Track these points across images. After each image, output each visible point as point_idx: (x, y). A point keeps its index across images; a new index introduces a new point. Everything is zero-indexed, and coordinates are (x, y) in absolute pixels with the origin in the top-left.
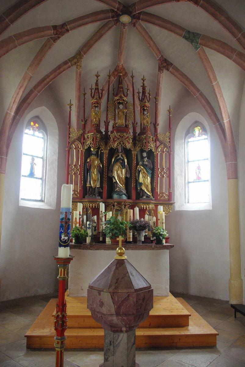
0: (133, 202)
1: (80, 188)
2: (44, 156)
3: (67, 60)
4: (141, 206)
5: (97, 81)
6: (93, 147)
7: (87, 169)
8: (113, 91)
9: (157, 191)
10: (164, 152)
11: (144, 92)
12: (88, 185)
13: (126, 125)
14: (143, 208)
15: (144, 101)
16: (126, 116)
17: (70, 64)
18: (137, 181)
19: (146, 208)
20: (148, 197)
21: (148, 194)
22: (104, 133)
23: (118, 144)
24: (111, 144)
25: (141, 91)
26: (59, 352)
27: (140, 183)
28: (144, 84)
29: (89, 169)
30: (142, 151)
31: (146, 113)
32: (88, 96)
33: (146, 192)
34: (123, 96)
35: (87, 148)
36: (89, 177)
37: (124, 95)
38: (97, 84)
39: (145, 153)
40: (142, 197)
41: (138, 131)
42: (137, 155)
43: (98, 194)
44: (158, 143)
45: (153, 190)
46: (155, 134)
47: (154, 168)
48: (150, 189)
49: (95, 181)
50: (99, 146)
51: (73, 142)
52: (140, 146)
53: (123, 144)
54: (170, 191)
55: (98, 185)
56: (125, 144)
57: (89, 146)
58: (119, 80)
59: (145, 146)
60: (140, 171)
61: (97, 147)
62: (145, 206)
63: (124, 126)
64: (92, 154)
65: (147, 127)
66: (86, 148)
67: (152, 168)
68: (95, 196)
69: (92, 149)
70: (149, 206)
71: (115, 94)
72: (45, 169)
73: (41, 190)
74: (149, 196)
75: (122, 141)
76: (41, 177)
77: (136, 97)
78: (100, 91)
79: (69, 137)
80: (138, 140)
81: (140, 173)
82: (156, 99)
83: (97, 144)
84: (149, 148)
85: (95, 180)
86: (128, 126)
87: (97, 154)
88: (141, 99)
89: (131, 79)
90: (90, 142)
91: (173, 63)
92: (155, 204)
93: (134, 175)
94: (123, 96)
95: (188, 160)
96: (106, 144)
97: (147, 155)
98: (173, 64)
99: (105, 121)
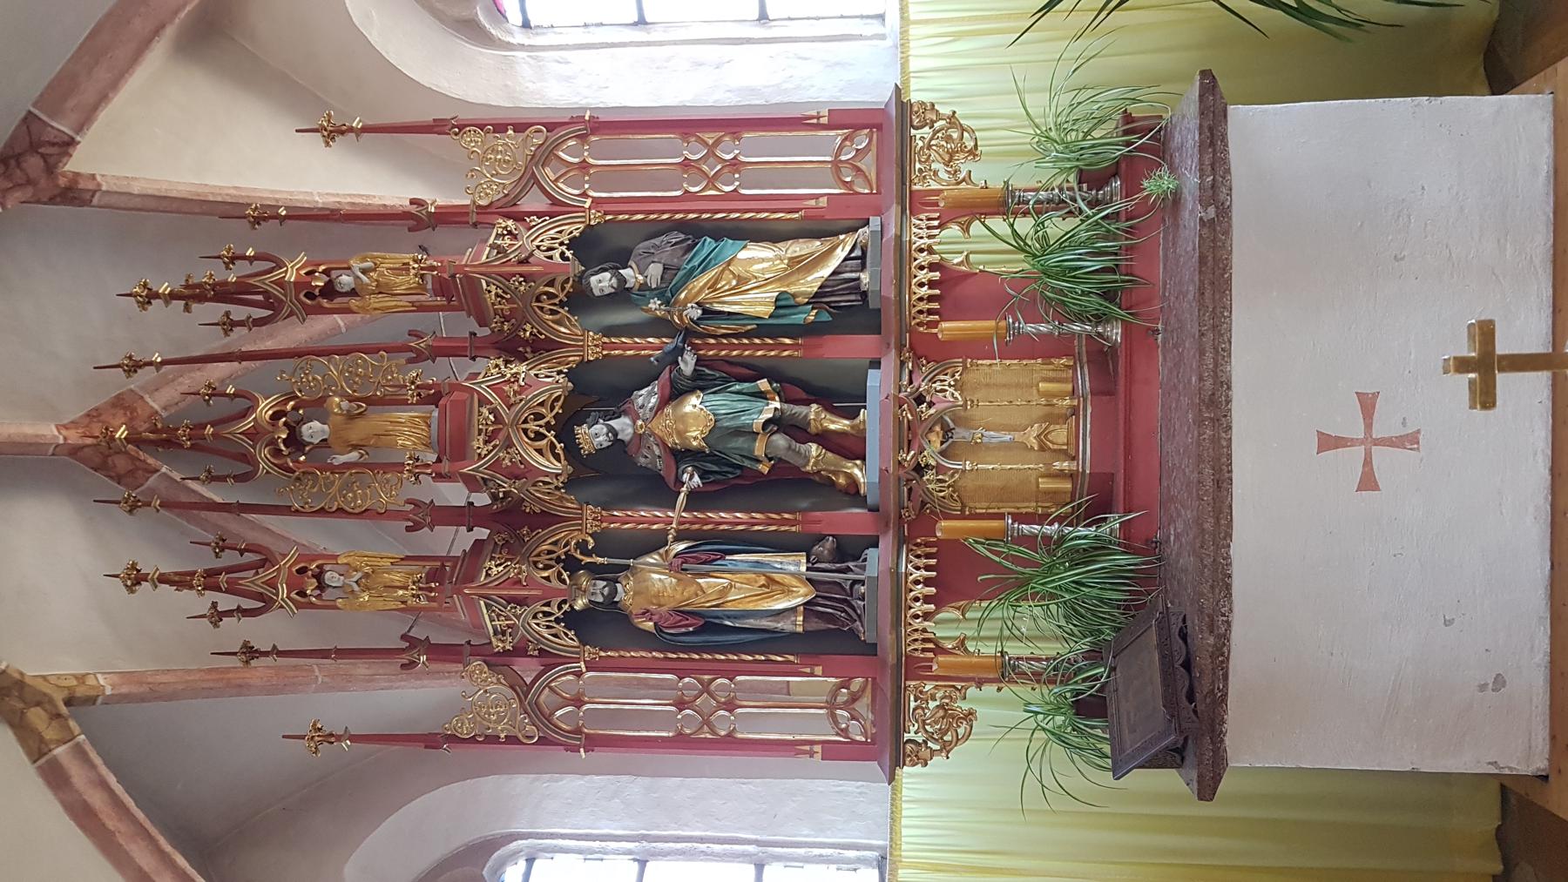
1: (818, 670)
2: (629, 852)
3: (39, 768)
4: (921, 299)
5: (163, 579)
6: (564, 602)
8: (222, 479)
9: (823, 202)
10: (584, 166)
11: (223, 293)
12: (798, 624)
13: (423, 401)
14: (932, 284)
15: (276, 291)
16: (371, 401)
17: (60, 751)
18: (764, 329)
19: (932, 267)
20: (863, 257)
21: (846, 259)
22: (482, 533)
23: (539, 451)
24: (545, 489)
25: (216, 310)
26: (464, 219)
27: (777, 308)
28: (173, 296)
30: (580, 300)
31: (346, 280)
32: (266, 630)
33: (834, 273)
34: (247, 424)
35: (571, 634)
36: (751, 623)
37: (244, 415)
38: (180, 581)
39: (593, 279)
40: (864, 294)
41: (455, 325)
42: (609, 331)
43: (851, 564)
44: (533, 202)
45: (819, 228)
46: (474, 218)
47: (682, 226)
48: (816, 245)
49: (772, 585)
50: (558, 560)
51: (540, 715)
52: (553, 312)
53: (539, 417)
54: (824, 120)
55: (798, 564)
56: (542, 404)
57: (557, 621)
58: (151, 442)
59: (549, 278)
60: (705, 311)
61: (565, 575)
62: (923, 276)
63: (436, 414)
64: (611, 602)
65: (432, 268)
66: (570, 641)
67: (682, 236)
68: (862, 582)
69: (580, 604)
70: (921, 250)
71: (242, 468)
72: (703, 847)
73: (823, 867)
74: (857, 253)
75: (525, 421)
76: (751, 869)
77: (271, 336)
78: (230, 558)
79: (512, 740)
80: (519, 327)
81: (718, 307)
82: (257, 220)
83: (545, 574)
84: (562, 254)
86: (429, 387)
87: (610, 574)
88: (267, 313)
89: (146, 374)
90: (535, 617)
91: (23, 114)
92: (903, 211)
93: (733, 347)
94: (247, 424)
95: (635, 24)
96: (546, 519)
97: (611, 264)
98: (30, 112)
99: (408, 529)
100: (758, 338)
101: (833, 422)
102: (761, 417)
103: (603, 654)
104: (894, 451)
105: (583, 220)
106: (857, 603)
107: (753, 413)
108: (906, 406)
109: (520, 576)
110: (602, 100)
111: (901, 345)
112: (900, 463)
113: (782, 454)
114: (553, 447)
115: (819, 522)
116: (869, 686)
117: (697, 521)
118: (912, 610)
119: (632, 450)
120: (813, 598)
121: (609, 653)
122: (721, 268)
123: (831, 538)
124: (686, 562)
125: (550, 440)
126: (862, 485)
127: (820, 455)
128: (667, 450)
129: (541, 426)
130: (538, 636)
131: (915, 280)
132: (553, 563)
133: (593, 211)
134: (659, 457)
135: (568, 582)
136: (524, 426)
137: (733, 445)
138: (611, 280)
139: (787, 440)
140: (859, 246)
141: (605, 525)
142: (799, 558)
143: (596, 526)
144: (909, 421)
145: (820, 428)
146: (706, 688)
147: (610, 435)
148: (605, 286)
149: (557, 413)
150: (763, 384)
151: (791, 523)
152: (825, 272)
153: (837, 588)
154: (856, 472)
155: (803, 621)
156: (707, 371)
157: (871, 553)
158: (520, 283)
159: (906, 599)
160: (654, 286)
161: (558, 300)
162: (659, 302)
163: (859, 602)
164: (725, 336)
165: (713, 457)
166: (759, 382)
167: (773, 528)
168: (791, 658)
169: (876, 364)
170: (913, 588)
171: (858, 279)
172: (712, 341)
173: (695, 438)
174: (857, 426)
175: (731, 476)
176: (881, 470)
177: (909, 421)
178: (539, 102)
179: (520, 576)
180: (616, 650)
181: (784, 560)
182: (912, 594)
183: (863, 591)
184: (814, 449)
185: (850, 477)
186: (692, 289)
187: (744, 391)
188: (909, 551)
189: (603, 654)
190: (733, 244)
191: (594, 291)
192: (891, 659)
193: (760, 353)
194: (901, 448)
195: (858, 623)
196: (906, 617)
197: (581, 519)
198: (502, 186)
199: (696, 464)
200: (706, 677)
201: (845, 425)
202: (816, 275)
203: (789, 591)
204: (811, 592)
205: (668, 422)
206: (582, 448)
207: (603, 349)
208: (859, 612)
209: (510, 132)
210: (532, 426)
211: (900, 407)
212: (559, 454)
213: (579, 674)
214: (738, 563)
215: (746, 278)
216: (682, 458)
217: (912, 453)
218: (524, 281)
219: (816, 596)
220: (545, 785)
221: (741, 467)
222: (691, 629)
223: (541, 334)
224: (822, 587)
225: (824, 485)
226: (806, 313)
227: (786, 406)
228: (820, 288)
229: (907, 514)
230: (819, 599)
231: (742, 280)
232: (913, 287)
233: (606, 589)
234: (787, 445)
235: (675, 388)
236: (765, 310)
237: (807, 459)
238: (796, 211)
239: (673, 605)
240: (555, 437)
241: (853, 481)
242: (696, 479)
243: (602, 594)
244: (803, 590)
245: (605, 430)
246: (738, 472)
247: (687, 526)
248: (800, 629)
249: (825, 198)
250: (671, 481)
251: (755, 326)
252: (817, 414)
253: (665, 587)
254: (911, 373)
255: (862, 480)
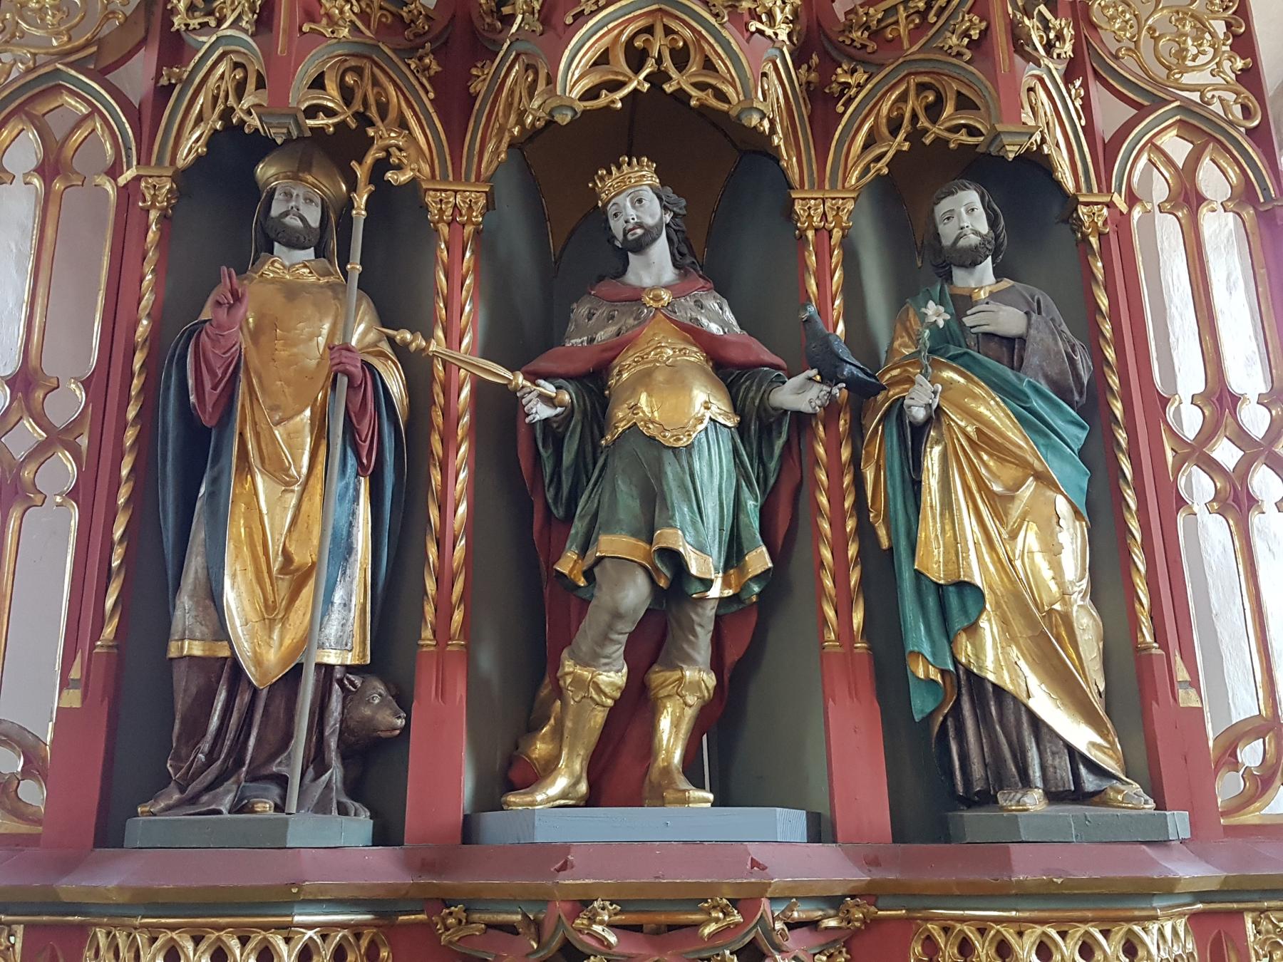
0: (859, 876)
7: (185, 410)
20: (1078, 796)
21: (1071, 750)
23: (603, 59)
29: (208, 419)
40: (987, 799)
43: (335, 773)
55: (342, 645)
56: (708, 65)
74: (1090, 782)
75: (668, 31)
81: (932, 458)
85: (298, 577)
93: (836, 496)
100: (860, 553)
101: (676, 725)
102: (689, 547)
103: (153, 215)
104: (620, 887)
105: (1084, 190)
106: (229, 792)
107: (697, 530)
108: (738, 918)
109: (324, 21)
110: (1181, 340)
111: (877, 897)
112: (587, 903)
113: (603, 597)
114: (615, 86)
115: (442, 692)
116: (23, 828)
117: (451, 419)
118: (190, 946)
119: (606, 288)
120: (250, 682)
121: (154, 227)
122: (1031, 459)
123: (400, 722)
124: (350, 385)
125: (630, 80)
126: (528, 799)
127: (599, 690)
128: (608, 355)
129: (659, 61)
130: (197, 80)
131: (1053, 932)
132: (357, 106)
133: (1105, 211)
134: (591, 341)
135: (310, 122)
136: (659, 31)
137: (622, 486)
138: (976, 233)
139: (635, 611)
140: (1105, 784)
141: (444, 229)
142: (357, 649)
143: (441, 211)
144: (697, 926)
145: (663, 693)
146: (56, 438)
147: (639, 231)
148: (960, 219)
149: (690, 97)
150: (759, 560)
151: (441, 630)
152: (1045, 704)
153: (273, 738)
154: (560, 784)
155: (191, 657)
156: (779, 444)
157: (360, 826)
158: (966, 34)
159: (220, 928)
160: (968, 321)
161: (927, 124)
162: (941, 324)
163: (228, 799)
164: (859, 481)
165: (590, 455)
166: (764, 549)
167: (431, 586)
168: (109, 631)
169: (819, 830)
170: (250, 946)
171: (1026, 783)
172: (845, 454)
173: (635, 408)
174: (672, 782)
175: (550, 496)
176: (566, 848)
177: (697, 926)
178: (1166, 244)
179: (324, 21)
180: (161, 244)
181: (354, 612)
182: (234, 944)
183: (259, 807)
184: (613, 678)
185: (548, 769)
186: (975, 397)
187: (742, 517)
188: (357, 930)
189: (153, 215)
190: (1081, 489)
191: (949, 199)
192: (70, 886)
193: (826, 554)
194: (624, 905)
195: (176, 796)
196: (173, 928)
197: (457, 178)
198: (1132, 46)
199: (577, 417)
200: (84, 441)
201: (669, 753)
202: (1034, 682)
203: (272, 621)
204: (264, 674)
205: (670, 352)
206: (610, 173)
207: (817, 230)
208: (205, 798)
209: (1239, 64)
210: (659, 44)
211: (734, 902)
212: (597, 97)
213: (113, 172)
214: (346, 505)
215: (1006, 514)
216: (590, 391)
217: (613, 939)
218: (971, 41)
219: (255, 692)
220: (13, 246)
221: (569, 518)
222: (192, 398)
223: (847, 105)
224: (280, 704)
225: (530, 711)
226: (934, 655)
227: (710, 611)
228: (999, 690)
229: (451, 921)
230: (247, 697)
231: (999, 504)
232: (1039, 929)
233: (299, 223)
234: (622, 610)
235: (740, 376)
236: (934, 564)
237: (591, 661)
238: (1159, 635)
239: (254, 360)
240: (635, 90)
241: (536, 776)
242: (542, 412)
243: (286, 214)
244: (272, 656)
245: (650, 221)
246: (559, 512)
247: (440, 399)
248: (173, 652)
249: (1200, 706)
250: (541, 364)
251: (885, 543)
252: (695, 686)
253: (295, 345)
254: (813, 924)
255: (540, 797)
